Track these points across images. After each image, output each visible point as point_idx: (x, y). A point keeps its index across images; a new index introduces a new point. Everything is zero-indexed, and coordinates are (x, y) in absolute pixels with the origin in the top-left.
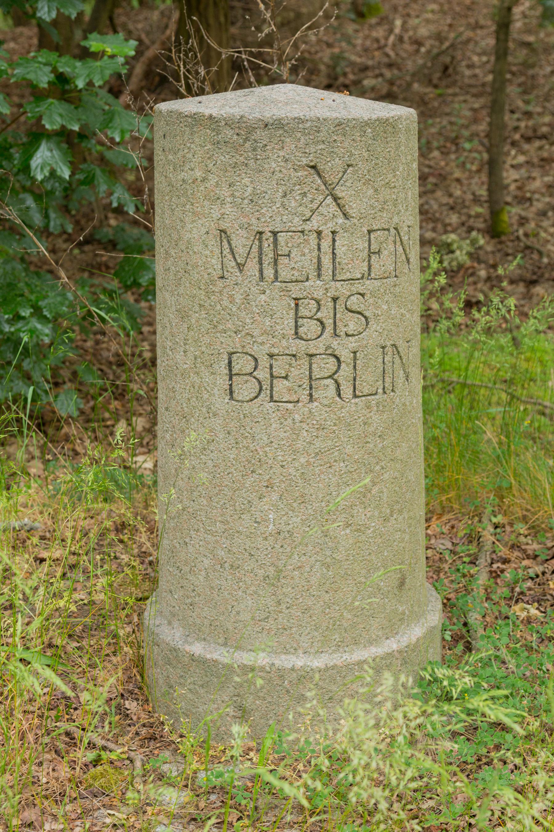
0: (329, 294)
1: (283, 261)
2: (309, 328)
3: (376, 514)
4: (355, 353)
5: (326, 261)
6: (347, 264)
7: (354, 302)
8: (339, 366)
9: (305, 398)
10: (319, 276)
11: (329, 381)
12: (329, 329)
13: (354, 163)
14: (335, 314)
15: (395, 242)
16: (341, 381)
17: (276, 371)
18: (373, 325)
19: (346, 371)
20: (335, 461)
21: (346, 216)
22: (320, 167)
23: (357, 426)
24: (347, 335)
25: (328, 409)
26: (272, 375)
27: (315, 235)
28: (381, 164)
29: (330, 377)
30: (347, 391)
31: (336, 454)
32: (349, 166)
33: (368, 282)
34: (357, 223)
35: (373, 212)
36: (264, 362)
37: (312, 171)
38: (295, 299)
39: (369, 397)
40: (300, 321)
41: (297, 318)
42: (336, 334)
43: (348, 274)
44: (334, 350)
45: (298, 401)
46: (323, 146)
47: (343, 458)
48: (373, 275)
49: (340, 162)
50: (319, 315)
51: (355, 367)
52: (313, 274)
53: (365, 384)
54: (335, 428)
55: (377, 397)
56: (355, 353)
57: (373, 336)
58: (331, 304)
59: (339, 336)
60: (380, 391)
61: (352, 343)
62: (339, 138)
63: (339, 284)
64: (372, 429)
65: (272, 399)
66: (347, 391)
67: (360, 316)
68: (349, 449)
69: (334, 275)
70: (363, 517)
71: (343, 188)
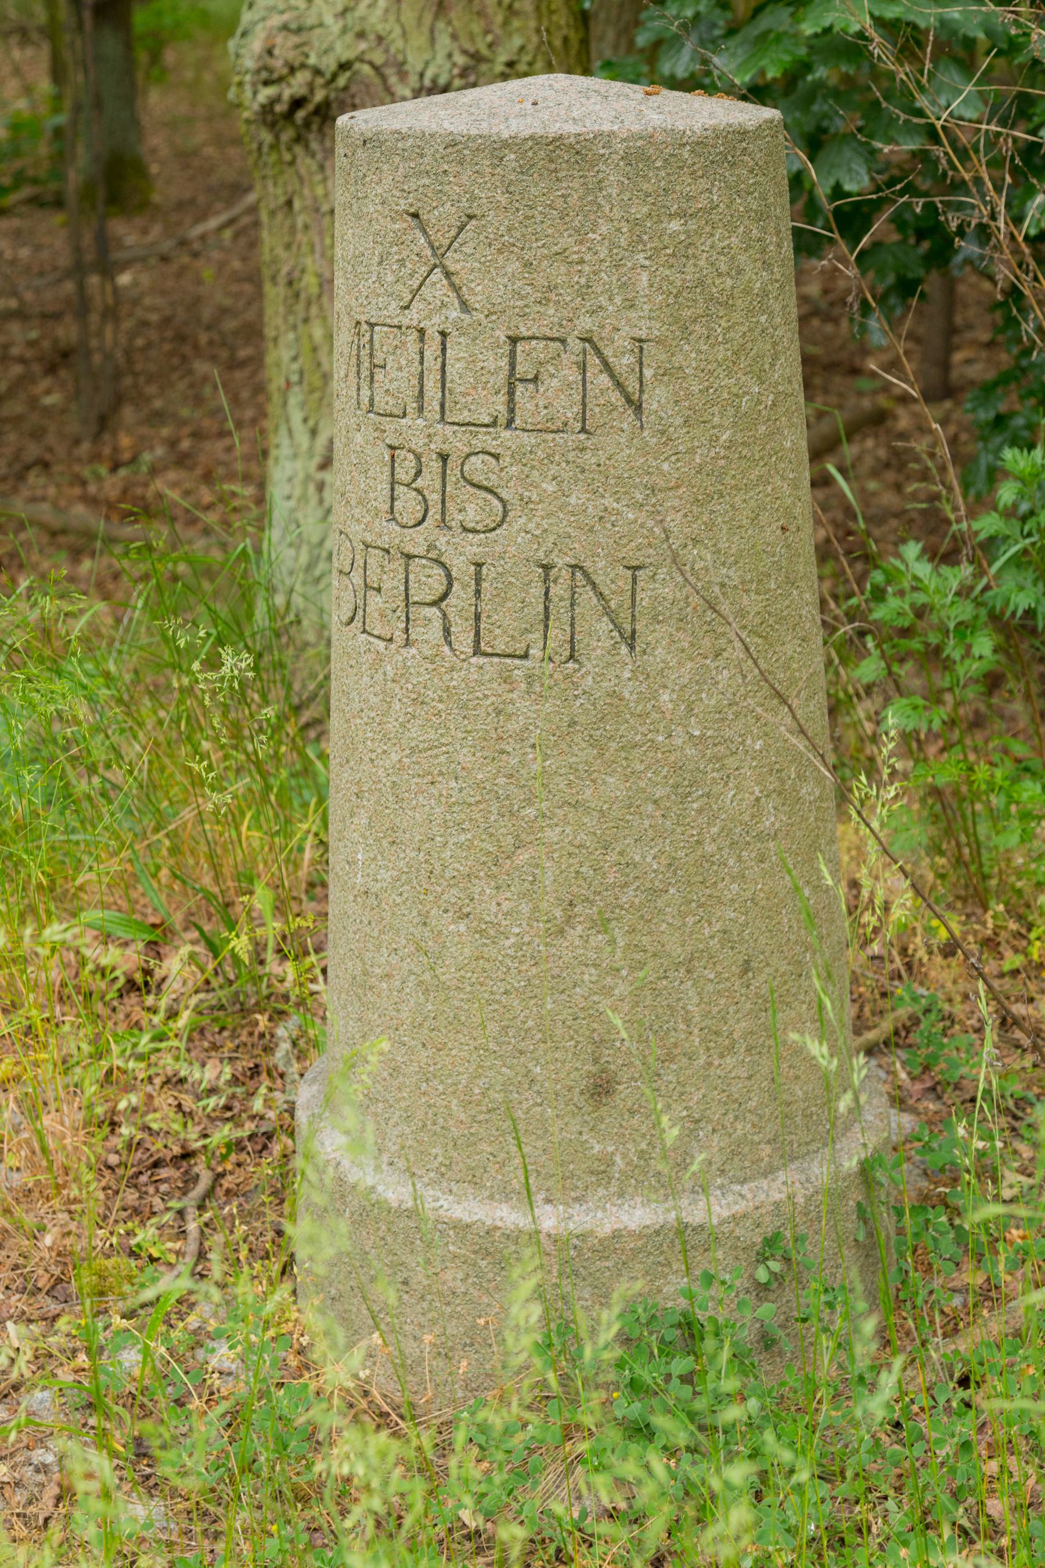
0: (433, 446)
1: (379, 375)
2: (408, 504)
3: (525, 908)
4: (479, 565)
6: (464, 394)
8: (450, 585)
9: (399, 637)
10: (421, 409)
11: (433, 612)
13: (478, 212)
14: (444, 485)
15: (583, 368)
16: (451, 613)
18: (518, 521)
19: (460, 598)
20: (441, 774)
21: (465, 306)
23: (481, 712)
24: (466, 530)
25: (431, 667)
27: (416, 334)
28: (539, 218)
29: (434, 604)
30: (464, 641)
31: (442, 759)
32: (470, 217)
33: (507, 434)
34: (484, 322)
35: (520, 303)
37: (413, 222)
38: (392, 448)
39: (508, 661)
41: (393, 483)
42: (443, 523)
43: (466, 413)
44: (441, 554)
45: (391, 640)
46: (427, 181)
47: (455, 771)
48: (518, 422)
49: (454, 210)
50: (419, 483)
51: (478, 592)
53: (498, 631)
54: (441, 706)
55: (527, 663)
56: (479, 565)
57: (517, 539)
59: (450, 528)
61: (473, 546)
62: (452, 168)
63: (449, 430)
64: (513, 726)
67: (489, 497)
68: (464, 756)
70: (494, 908)
71: (457, 256)
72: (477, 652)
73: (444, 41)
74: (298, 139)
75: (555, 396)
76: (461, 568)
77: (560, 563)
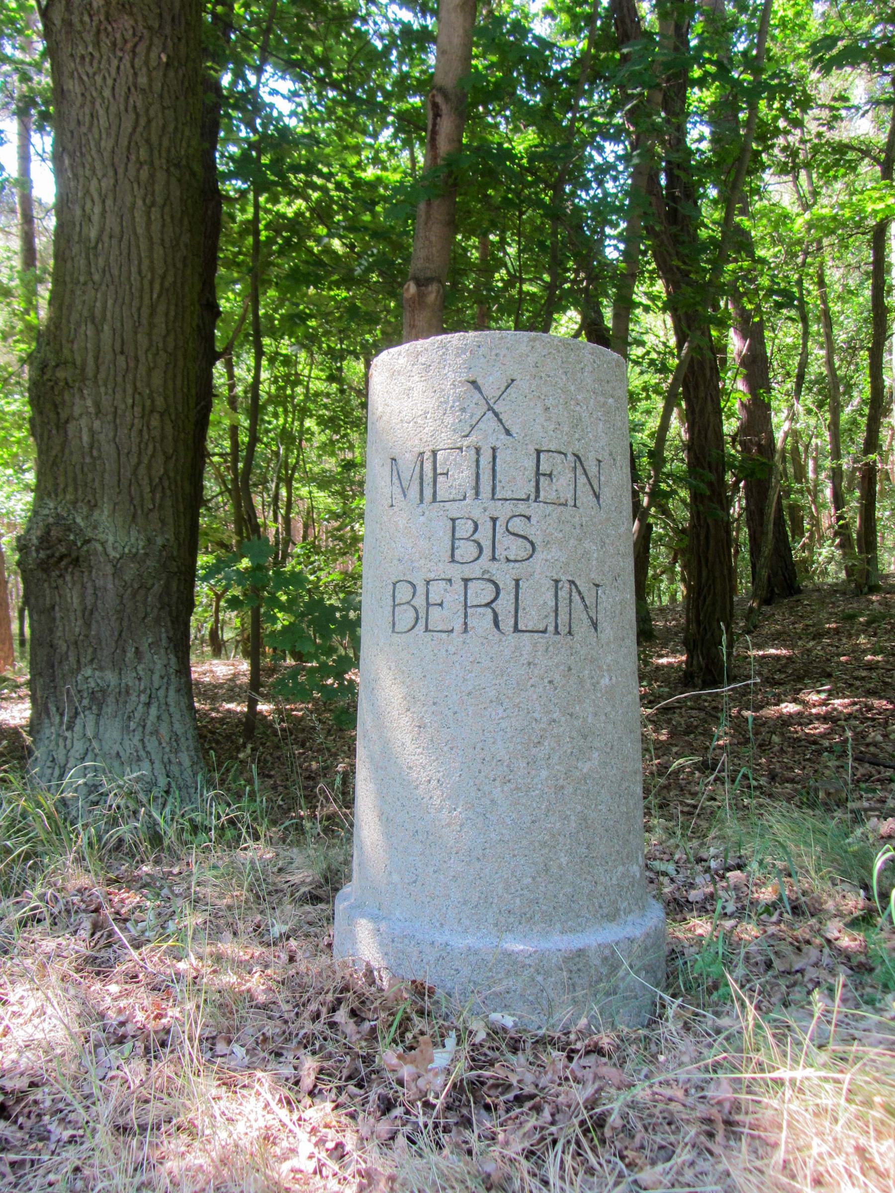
1: (440, 479)
2: (466, 550)
5: (486, 478)
7: (517, 525)
10: (477, 494)
12: (487, 552)
17: (434, 598)
18: (539, 556)
22: (480, 381)
24: (508, 560)
26: (428, 604)
29: (488, 605)
30: (507, 623)
36: (421, 590)
40: (457, 543)
50: (476, 537)
52: (470, 493)
58: (489, 524)
60: (551, 628)
61: (514, 570)
65: (427, 630)
66: (507, 623)
69: (493, 494)
72: (516, 629)
73: (134, 533)
74: (61, 576)
75: (561, 485)
76: (506, 584)
77: (564, 578)
